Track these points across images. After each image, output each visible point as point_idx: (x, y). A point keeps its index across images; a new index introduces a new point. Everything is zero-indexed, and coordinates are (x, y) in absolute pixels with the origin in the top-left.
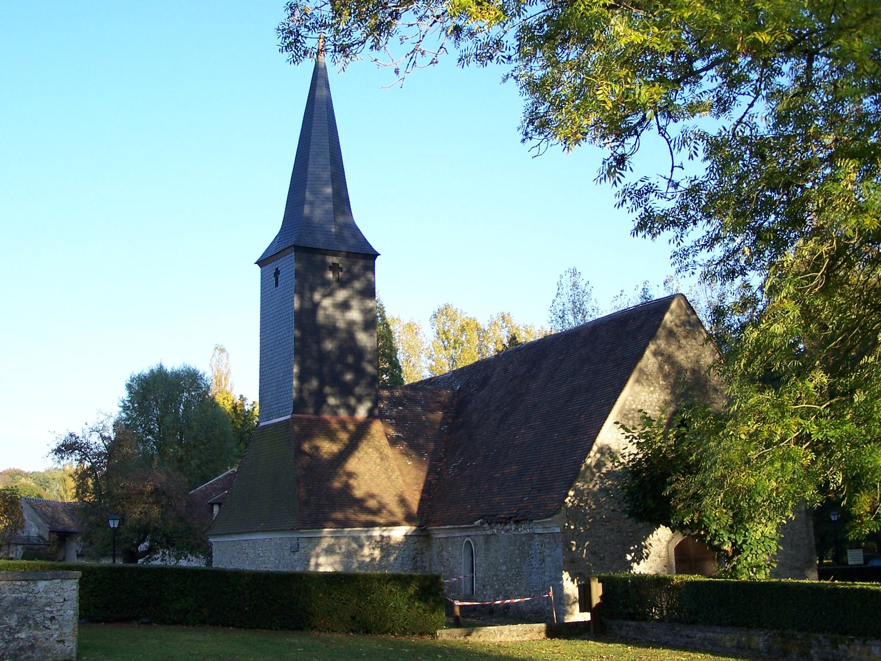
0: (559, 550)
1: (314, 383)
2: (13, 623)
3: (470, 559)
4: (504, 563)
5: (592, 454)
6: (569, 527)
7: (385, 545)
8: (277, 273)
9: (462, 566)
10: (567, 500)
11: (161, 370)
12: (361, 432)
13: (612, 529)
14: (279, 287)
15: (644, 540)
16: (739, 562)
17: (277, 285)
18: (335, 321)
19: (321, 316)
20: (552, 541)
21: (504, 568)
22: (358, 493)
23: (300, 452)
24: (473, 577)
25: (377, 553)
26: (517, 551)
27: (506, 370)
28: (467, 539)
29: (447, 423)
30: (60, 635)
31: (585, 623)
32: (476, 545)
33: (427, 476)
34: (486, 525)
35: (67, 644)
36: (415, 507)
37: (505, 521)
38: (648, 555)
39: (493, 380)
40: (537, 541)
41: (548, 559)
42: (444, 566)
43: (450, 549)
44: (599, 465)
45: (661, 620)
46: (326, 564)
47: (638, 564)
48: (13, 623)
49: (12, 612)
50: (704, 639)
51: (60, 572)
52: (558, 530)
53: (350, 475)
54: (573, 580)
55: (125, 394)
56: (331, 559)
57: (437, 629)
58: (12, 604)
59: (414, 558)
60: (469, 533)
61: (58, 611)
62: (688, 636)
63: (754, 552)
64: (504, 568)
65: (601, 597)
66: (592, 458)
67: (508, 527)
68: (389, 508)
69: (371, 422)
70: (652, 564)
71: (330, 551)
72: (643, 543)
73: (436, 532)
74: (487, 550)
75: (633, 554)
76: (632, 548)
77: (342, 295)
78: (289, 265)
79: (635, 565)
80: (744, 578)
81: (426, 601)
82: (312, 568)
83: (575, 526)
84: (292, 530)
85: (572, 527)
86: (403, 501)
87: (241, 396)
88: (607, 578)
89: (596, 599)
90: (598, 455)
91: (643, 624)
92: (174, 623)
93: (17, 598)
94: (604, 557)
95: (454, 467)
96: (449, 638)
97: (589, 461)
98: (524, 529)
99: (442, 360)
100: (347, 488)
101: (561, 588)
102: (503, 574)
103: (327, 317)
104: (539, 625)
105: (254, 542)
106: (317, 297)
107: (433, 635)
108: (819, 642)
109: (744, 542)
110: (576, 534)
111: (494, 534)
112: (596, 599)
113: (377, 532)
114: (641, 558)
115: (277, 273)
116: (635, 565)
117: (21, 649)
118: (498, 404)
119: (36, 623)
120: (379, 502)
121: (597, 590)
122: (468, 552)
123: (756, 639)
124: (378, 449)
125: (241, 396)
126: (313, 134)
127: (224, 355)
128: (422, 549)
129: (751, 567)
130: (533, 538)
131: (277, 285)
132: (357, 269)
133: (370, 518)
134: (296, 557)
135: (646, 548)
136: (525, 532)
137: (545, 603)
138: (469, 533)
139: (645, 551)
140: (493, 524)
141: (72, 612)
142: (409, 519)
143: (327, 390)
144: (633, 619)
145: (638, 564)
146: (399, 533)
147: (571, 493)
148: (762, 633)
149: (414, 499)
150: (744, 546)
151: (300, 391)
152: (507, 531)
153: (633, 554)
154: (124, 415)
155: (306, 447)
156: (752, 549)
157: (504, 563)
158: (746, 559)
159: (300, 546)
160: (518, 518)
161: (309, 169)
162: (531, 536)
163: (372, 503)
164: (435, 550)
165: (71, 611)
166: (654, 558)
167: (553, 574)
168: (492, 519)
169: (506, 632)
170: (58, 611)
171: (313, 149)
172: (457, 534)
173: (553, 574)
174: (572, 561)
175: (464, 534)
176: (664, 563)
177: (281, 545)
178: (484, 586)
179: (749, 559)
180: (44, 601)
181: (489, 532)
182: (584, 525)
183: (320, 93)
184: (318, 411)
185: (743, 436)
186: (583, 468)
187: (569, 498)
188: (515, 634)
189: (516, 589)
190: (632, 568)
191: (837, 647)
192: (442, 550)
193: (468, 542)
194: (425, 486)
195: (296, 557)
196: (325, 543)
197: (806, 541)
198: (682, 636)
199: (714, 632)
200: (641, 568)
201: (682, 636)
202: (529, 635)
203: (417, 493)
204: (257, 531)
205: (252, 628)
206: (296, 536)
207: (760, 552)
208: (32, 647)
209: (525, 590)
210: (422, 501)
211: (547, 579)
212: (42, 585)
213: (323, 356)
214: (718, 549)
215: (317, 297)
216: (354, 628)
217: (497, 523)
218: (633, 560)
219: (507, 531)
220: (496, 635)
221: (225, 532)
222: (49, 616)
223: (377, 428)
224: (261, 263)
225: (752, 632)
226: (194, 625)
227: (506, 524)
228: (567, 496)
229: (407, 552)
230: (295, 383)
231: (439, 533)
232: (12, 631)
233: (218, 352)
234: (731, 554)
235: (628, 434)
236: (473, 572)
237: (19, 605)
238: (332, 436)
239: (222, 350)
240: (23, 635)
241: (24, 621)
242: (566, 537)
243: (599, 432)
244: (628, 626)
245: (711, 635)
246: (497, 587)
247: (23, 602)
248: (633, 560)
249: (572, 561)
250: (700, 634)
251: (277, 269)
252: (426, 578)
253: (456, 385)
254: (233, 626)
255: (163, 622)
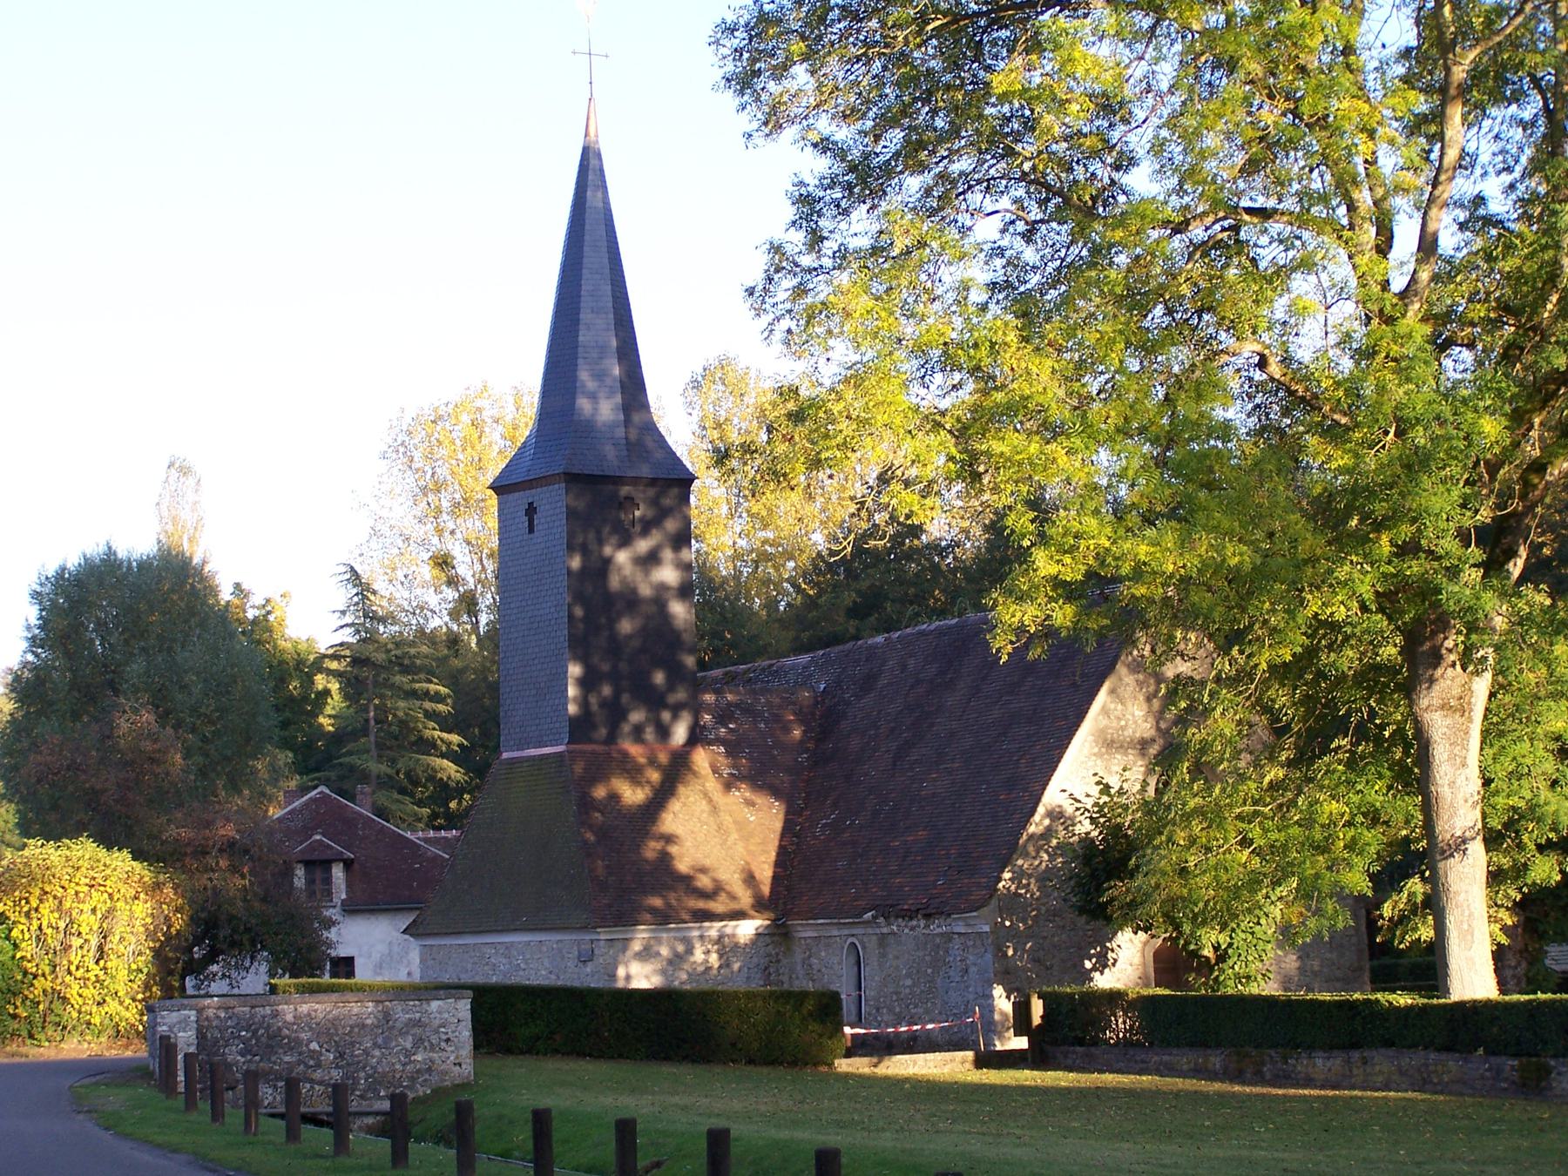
0: (989, 956)
1: (607, 690)
2: (409, 1046)
3: (856, 969)
4: (908, 975)
5: (1037, 818)
6: (1003, 923)
7: (726, 947)
8: (531, 510)
9: (844, 978)
10: (1000, 885)
11: (110, 552)
12: (677, 771)
13: (1064, 927)
14: (536, 534)
15: (1110, 940)
16: (1222, 971)
17: (531, 530)
18: (634, 591)
19: (614, 582)
20: (978, 942)
21: (909, 982)
22: (682, 866)
23: (587, 804)
24: (860, 996)
25: (714, 959)
26: (927, 958)
27: (904, 667)
28: (850, 940)
29: (807, 750)
30: (457, 1057)
31: (1021, 1051)
32: (864, 948)
33: (781, 840)
34: (881, 920)
35: (464, 1066)
36: (766, 889)
37: (910, 915)
38: (1115, 960)
39: (882, 682)
40: (957, 943)
41: (973, 969)
42: (813, 981)
43: (823, 954)
44: (1048, 833)
45: (1117, 1044)
46: (640, 976)
47: (1102, 973)
48: (409, 1046)
49: (407, 1033)
50: (1161, 1064)
51: (453, 991)
52: (987, 928)
53: (669, 839)
54: (1008, 997)
55: (32, 613)
56: (648, 968)
57: (835, 1057)
58: (406, 1025)
59: (766, 968)
60: (854, 931)
61: (453, 1032)
62: (1143, 1061)
63: (1243, 958)
64: (909, 982)
65: (1042, 1017)
66: (1038, 822)
67: (914, 923)
68: (727, 887)
69: (685, 745)
70: (1120, 976)
71: (646, 954)
72: (1108, 944)
73: (800, 929)
74: (883, 955)
75: (1094, 960)
76: (1093, 951)
77: (643, 546)
78: (554, 502)
79: (1096, 975)
80: (1230, 991)
81: (823, 1022)
82: (620, 984)
83: (1011, 921)
84: (584, 928)
85: (1008, 923)
86: (750, 879)
87: (237, 586)
88: (1050, 993)
89: (1036, 1020)
90: (1047, 822)
91: (1093, 1049)
92: (522, 1053)
93: (410, 1019)
94: (1052, 966)
95: (824, 825)
96: (850, 1070)
97: (1032, 829)
98: (938, 927)
99: (712, 493)
100: (665, 859)
101: (991, 1009)
102: (907, 991)
103: (623, 581)
104: (962, 1053)
105: (509, 946)
106: (608, 550)
107: (831, 1065)
108: (1271, 1057)
109: (1230, 945)
110: (1012, 933)
111: (893, 933)
112: (1036, 1020)
113: (713, 929)
114: (1105, 966)
115: (531, 510)
116: (1096, 975)
117: (418, 1071)
118: (892, 725)
119: (432, 1045)
120: (715, 880)
121: (1037, 1008)
122: (852, 960)
123: (1212, 1059)
124: (706, 795)
125: (237, 586)
126: (584, 277)
127: (191, 481)
128: (777, 954)
129: (1238, 977)
130: (950, 940)
131: (531, 530)
132: (667, 502)
133: (701, 904)
134: (588, 970)
135: (1113, 950)
136: (939, 930)
137: (969, 1030)
138: (854, 931)
139: (1110, 955)
140: (892, 919)
141: (468, 1034)
142: (760, 905)
143: (625, 698)
144: (1081, 1045)
145: (1102, 973)
146: (746, 929)
147: (1007, 875)
148: (1218, 1052)
149: (765, 873)
150: (1230, 951)
151: (584, 703)
152: (912, 929)
153: (1094, 960)
154: (30, 657)
155: (600, 792)
156: (1240, 955)
157: (908, 975)
158: (1233, 968)
159: (596, 952)
160: (928, 911)
161: (581, 338)
162: (948, 937)
163: (704, 882)
164: (799, 956)
165: (466, 1033)
166: (1124, 966)
167: (980, 990)
168: (889, 910)
169: (921, 1062)
170: (453, 1032)
171: (586, 303)
172: (835, 933)
173: (980, 990)
174: (1007, 972)
175: (846, 932)
176: (1138, 973)
177: (560, 950)
178: (878, 1010)
179: (1236, 967)
180: (437, 1022)
181: (885, 930)
182: (1024, 921)
183: (593, 197)
184: (612, 738)
185: (1182, 843)
186: (1025, 837)
187: (1003, 883)
188: (932, 1064)
189: (927, 1012)
190: (1091, 980)
191: (1286, 1063)
192: (810, 957)
193: (853, 944)
194: (778, 855)
195: (588, 970)
196: (637, 946)
197: (1354, 940)
198: (1136, 1062)
199: (1170, 1055)
200: (1104, 981)
201: (1136, 1062)
202: (949, 1066)
203: (766, 866)
204: (516, 930)
205: (612, 1058)
206: (588, 937)
207: (1250, 958)
208: (429, 1070)
209: (940, 1013)
210: (776, 878)
211: (971, 997)
212: (435, 1005)
213: (615, 646)
214: (1195, 954)
215: (608, 550)
216: (734, 1057)
217: (897, 917)
218: (1094, 969)
219: (912, 929)
220: (908, 1066)
221: (444, 931)
222: (444, 1037)
223: (701, 758)
224: (499, 488)
225: (1209, 1051)
226: (546, 1054)
227: (911, 919)
228: (1000, 880)
229: (755, 960)
230: (572, 691)
231: (805, 931)
232: (408, 1054)
233: (173, 473)
234: (1213, 961)
235: (1079, 805)
236: (860, 989)
237: (414, 1026)
238: (634, 773)
239: (185, 471)
240: (419, 1057)
241: (419, 1042)
242: (999, 938)
243: (1044, 789)
244: (1074, 1052)
245: (1166, 1058)
246: (897, 1010)
247: (418, 1023)
248: (1094, 969)
249: (1007, 972)
250: (1156, 1058)
251: (530, 504)
252: (823, 994)
253: (818, 682)
254: (590, 1055)
255: (509, 1051)
